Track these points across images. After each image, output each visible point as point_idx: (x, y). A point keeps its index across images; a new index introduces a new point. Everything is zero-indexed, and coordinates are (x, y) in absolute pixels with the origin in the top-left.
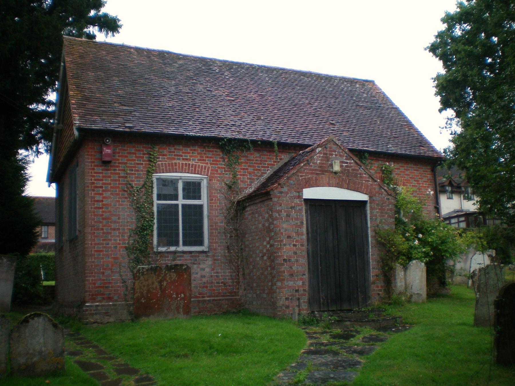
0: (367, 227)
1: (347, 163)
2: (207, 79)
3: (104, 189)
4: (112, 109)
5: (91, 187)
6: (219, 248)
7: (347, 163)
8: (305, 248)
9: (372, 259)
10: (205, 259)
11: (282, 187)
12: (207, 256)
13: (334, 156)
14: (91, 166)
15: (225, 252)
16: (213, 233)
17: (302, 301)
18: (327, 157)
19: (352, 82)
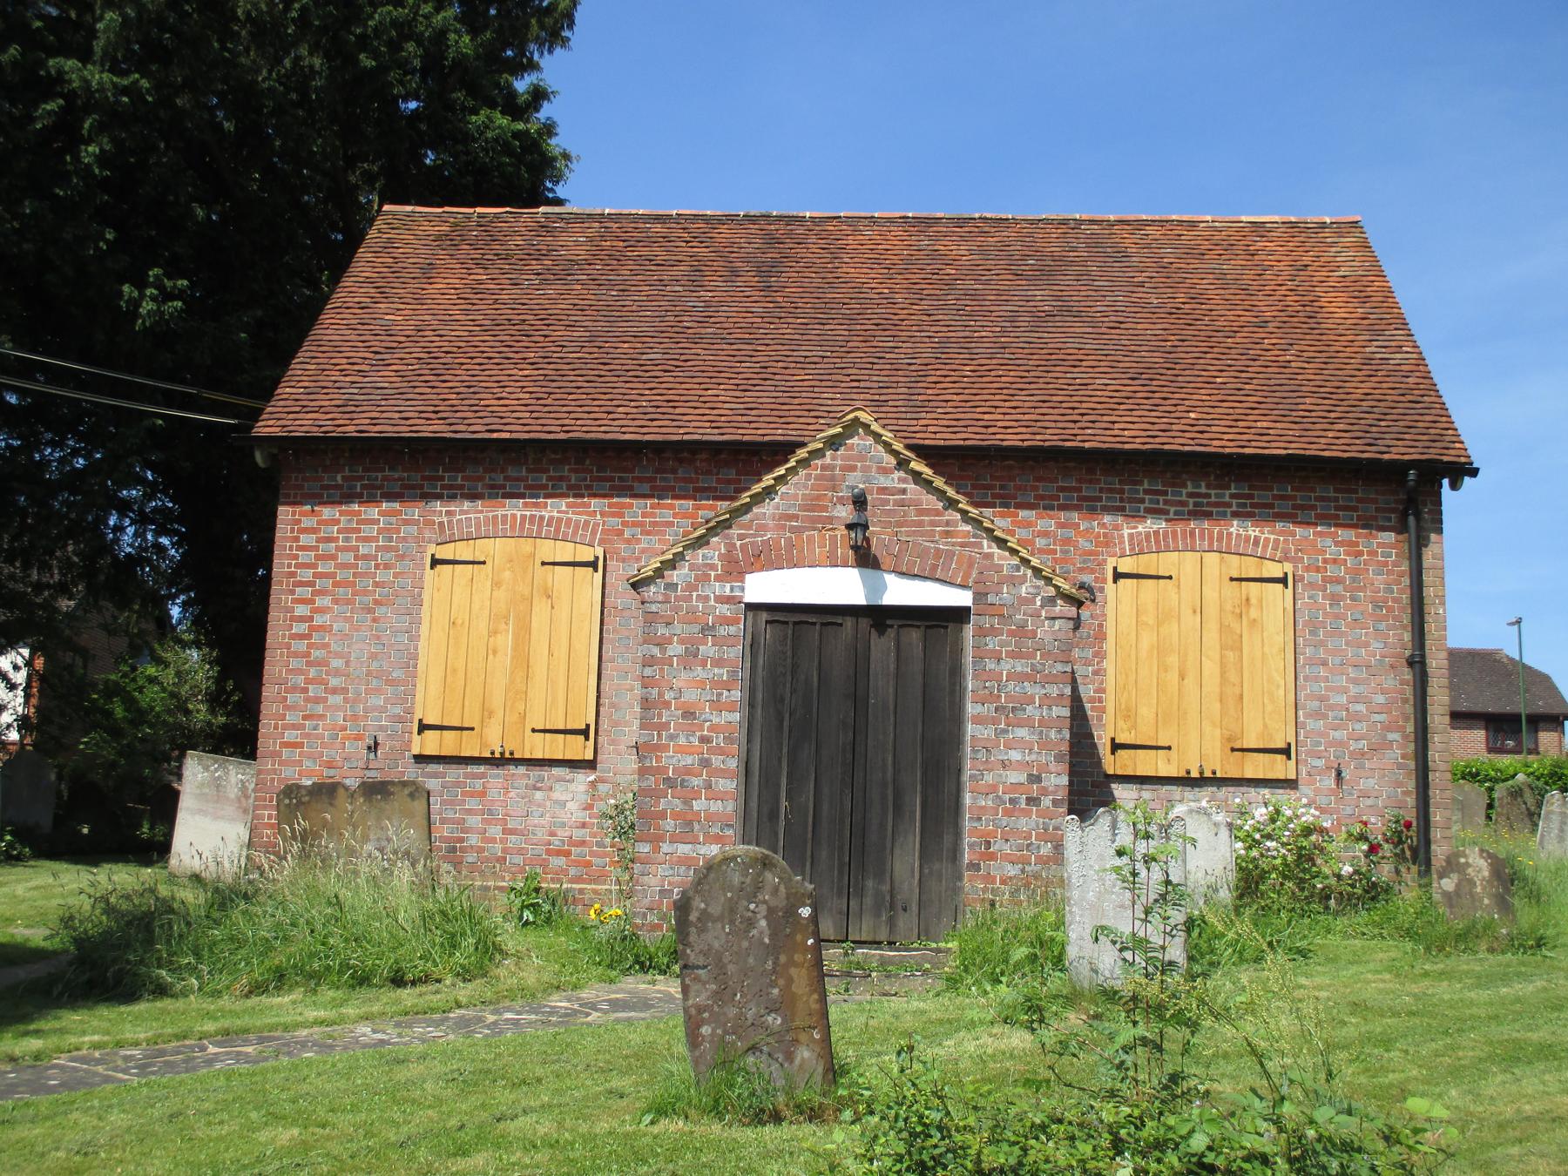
5: (288, 585)
14: (292, 531)
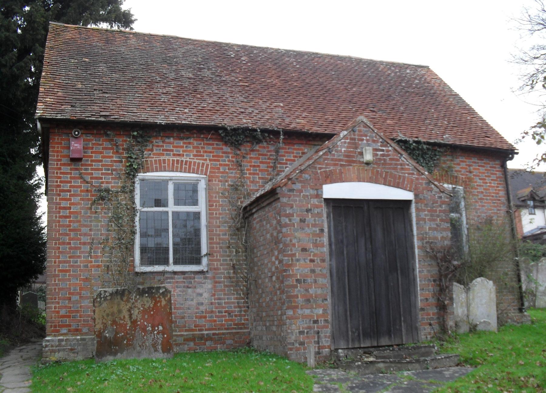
0: (413, 235)
1: (383, 150)
2: (218, 64)
3: (72, 193)
4: (89, 97)
5: (57, 191)
6: (222, 267)
7: (383, 150)
8: (326, 264)
9: (420, 278)
10: (203, 282)
11: (293, 184)
12: (206, 278)
13: (365, 142)
14: (57, 165)
15: (229, 273)
16: (213, 248)
17: (322, 335)
18: (355, 144)
19: (401, 67)
